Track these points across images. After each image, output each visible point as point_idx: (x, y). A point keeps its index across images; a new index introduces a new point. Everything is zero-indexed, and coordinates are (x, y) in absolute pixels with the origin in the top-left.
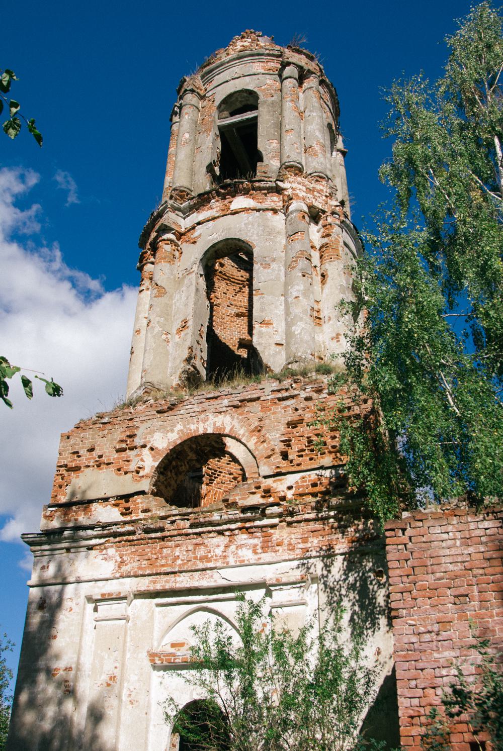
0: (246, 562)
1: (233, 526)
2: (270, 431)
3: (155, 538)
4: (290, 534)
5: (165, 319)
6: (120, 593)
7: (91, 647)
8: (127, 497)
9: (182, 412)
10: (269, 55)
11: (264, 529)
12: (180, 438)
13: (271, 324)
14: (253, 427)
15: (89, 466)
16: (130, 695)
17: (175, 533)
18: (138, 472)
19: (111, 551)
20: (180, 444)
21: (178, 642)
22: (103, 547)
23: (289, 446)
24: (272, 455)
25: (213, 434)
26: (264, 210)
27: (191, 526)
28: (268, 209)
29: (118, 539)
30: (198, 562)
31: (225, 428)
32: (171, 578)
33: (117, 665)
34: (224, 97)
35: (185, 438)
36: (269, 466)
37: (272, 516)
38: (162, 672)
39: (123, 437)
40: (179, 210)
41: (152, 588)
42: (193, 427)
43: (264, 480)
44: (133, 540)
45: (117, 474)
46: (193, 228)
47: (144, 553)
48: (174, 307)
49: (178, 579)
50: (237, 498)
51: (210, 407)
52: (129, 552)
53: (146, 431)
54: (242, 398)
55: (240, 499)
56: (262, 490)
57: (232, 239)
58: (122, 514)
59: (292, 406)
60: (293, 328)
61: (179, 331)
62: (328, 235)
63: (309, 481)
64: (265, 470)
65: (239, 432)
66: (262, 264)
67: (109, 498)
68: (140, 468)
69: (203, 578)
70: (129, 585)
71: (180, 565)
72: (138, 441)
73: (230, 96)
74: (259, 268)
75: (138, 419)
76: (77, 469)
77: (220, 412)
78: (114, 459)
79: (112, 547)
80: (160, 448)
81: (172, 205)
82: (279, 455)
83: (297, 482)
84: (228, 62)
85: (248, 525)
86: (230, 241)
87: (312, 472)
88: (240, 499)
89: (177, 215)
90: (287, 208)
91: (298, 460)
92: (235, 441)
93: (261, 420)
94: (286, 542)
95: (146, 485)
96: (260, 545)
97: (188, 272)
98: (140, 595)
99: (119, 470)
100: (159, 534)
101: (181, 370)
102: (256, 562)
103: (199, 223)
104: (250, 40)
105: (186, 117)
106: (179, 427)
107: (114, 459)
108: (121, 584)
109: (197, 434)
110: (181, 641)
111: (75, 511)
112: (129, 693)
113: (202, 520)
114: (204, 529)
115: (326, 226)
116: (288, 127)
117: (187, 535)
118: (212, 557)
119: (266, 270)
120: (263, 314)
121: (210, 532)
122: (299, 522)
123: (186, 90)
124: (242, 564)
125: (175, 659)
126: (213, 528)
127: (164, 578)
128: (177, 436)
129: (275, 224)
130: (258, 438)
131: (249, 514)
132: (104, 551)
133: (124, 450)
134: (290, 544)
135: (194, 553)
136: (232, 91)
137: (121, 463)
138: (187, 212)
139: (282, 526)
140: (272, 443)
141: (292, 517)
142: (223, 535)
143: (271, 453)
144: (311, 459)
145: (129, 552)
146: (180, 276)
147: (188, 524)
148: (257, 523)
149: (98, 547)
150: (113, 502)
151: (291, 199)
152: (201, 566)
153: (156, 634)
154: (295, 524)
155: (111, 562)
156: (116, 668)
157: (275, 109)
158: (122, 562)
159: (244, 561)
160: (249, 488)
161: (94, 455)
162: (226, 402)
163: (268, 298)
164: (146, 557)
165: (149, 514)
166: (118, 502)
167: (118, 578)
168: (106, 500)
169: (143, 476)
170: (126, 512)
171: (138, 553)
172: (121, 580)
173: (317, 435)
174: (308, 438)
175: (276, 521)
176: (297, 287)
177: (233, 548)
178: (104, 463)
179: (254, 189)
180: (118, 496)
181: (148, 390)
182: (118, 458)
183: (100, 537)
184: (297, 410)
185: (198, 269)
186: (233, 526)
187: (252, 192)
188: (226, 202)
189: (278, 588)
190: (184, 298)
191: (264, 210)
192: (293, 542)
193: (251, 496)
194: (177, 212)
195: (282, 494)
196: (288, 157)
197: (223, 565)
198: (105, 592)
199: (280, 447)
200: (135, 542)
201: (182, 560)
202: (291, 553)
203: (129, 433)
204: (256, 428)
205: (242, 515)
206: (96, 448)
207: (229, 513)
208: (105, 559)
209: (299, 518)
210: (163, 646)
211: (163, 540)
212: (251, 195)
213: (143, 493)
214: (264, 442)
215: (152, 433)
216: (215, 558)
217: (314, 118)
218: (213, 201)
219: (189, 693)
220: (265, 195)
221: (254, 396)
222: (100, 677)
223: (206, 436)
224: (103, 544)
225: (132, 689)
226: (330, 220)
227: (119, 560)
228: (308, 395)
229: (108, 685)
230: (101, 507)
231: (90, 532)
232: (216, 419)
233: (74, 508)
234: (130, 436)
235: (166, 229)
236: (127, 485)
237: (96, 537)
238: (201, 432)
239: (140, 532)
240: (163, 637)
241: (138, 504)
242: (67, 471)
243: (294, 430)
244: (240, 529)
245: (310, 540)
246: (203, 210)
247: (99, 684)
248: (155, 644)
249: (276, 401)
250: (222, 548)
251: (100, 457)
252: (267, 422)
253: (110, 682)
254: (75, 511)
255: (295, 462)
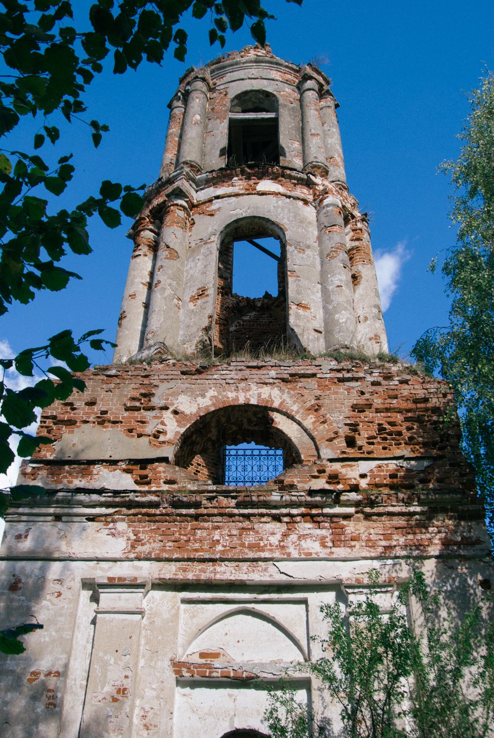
0: (314, 556)
1: (294, 511)
2: (331, 411)
3: (186, 515)
4: (368, 528)
5: (177, 283)
6: (136, 579)
7: (85, 648)
8: (144, 463)
9: (215, 376)
10: (287, 67)
11: (335, 520)
12: (214, 404)
13: (309, 309)
14: (308, 404)
15: (87, 422)
16: (144, 717)
17: (216, 511)
18: (156, 436)
19: (122, 526)
20: (213, 412)
21: (210, 651)
22: (109, 519)
23: (355, 430)
24: (334, 438)
25: (257, 406)
26: (294, 198)
27: (238, 506)
28: (298, 199)
29: (132, 511)
30: (246, 551)
31: (273, 402)
32: (209, 567)
33: (129, 673)
34: (240, 92)
35: (221, 406)
36: (333, 449)
37: (347, 504)
38: (188, 690)
39: (136, 394)
40: (194, 180)
41: (182, 577)
42: (231, 395)
43: (329, 464)
44: (155, 515)
45: (127, 435)
46: (210, 201)
47: (168, 532)
48: (185, 274)
49: (218, 569)
50: (295, 480)
51: (252, 376)
52: (146, 529)
53: (167, 392)
54: (294, 372)
55: (298, 482)
56: (327, 474)
57: (260, 218)
58: (136, 482)
59: (357, 389)
60: (337, 316)
61: (193, 299)
62: (358, 239)
63: (387, 471)
64: (327, 452)
65: (292, 408)
66: (296, 248)
67: (117, 461)
68: (159, 432)
69: (253, 571)
70: (147, 570)
71: (220, 551)
72: (156, 401)
73: (246, 93)
74: (293, 251)
75: (156, 377)
76: (71, 423)
77: (266, 384)
78: (123, 418)
79: (123, 520)
80: (188, 412)
81: (187, 173)
82: (343, 439)
83: (371, 471)
84: (244, 63)
85: (314, 511)
86: (256, 220)
87: (390, 462)
88: (298, 482)
89: (191, 185)
90: (321, 201)
91: (367, 448)
92: (285, 418)
93: (319, 399)
94: (364, 537)
95: (169, 452)
96: (330, 537)
97: (204, 242)
98: (159, 585)
99: (130, 431)
100: (192, 511)
101: (198, 339)
102: (326, 556)
103: (217, 197)
104: (264, 52)
105: (197, 100)
106: (212, 393)
107: (123, 418)
108: (136, 568)
109: (236, 403)
110: (214, 649)
111: (68, 472)
112: (142, 713)
113: (254, 498)
114: (255, 511)
115: (356, 230)
116: (313, 131)
117: (231, 515)
118: (265, 545)
119: (301, 255)
120: (300, 297)
121: (262, 515)
122: (380, 515)
123: (197, 77)
124: (309, 558)
125: (210, 673)
126: (268, 511)
127: (199, 566)
128: (210, 403)
129: (306, 214)
130: (317, 417)
131: (318, 499)
132: (111, 525)
133: (137, 409)
134: (369, 540)
135: (240, 538)
136: (249, 88)
137: (133, 424)
138: (200, 185)
139: (358, 518)
140: (335, 425)
141: (372, 508)
142: (280, 521)
143: (333, 436)
144: (384, 448)
145: (146, 529)
146: (193, 245)
147: (233, 502)
148: (327, 510)
149: (103, 519)
150: (124, 467)
151: (327, 193)
152: (251, 555)
153: (181, 639)
154: (375, 518)
155: (121, 539)
156: (126, 677)
157: (296, 114)
158: (138, 541)
159: (311, 554)
160: (310, 471)
161: (96, 410)
162: (273, 373)
163: (304, 282)
164: (173, 538)
165: (175, 486)
166: (130, 467)
167: (132, 560)
168: (113, 463)
169: (164, 442)
170: (143, 480)
171: (160, 532)
172: (136, 563)
173: (390, 423)
174: (379, 425)
175: (352, 510)
176: (339, 277)
177: (293, 537)
178: (109, 421)
179: (283, 176)
180: (130, 460)
181: (162, 351)
182: (129, 417)
183: (108, 505)
184: (363, 393)
185: (214, 247)
186: (294, 511)
187: (280, 178)
188: (251, 182)
189: (356, 590)
190: (200, 265)
191: (294, 198)
192: (373, 537)
193: (314, 480)
194: (191, 182)
195: (354, 482)
196: (316, 157)
197: (282, 556)
198: (111, 576)
199: (344, 431)
200: (157, 518)
201: (223, 546)
202: (372, 550)
203: (143, 391)
204: (313, 406)
205: (309, 499)
206: (98, 402)
207: (293, 493)
208: (113, 535)
209: (381, 510)
210: (190, 653)
211: (197, 520)
212: (280, 181)
213: (165, 460)
214: (324, 422)
215: (176, 394)
216: (269, 547)
217: (334, 133)
218: (236, 178)
219: (228, 719)
220: (295, 185)
221: (309, 372)
222: (102, 688)
223: (247, 407)
224: (110, 515)
225: (147, 709)
226: (359, 225)
227: (134, 538)
228: (376, 379)
229: (115, 700)
230: (106, 470)
231: (95, 497)
232: (260, 390)
233: (67, 468)
234: (144, 395)
235: (179, 193)
236: (143, 449)
237: (101, 505)
238: (242, 401)
239: (166, 505)
240: (190, 643)
241: (160, 472)
242: (55, 424)
243: (362, 415)
244: (303, 515)
245: (395, 537)
246: (223, 186)
247: (100, 698)
248: (180, 650)
249: (336, 380)
250: (279, 536)
251: (105, 412)
252: (327, 401)
253: (116, 696)
254: (68, 472)
255: (365, 449)
